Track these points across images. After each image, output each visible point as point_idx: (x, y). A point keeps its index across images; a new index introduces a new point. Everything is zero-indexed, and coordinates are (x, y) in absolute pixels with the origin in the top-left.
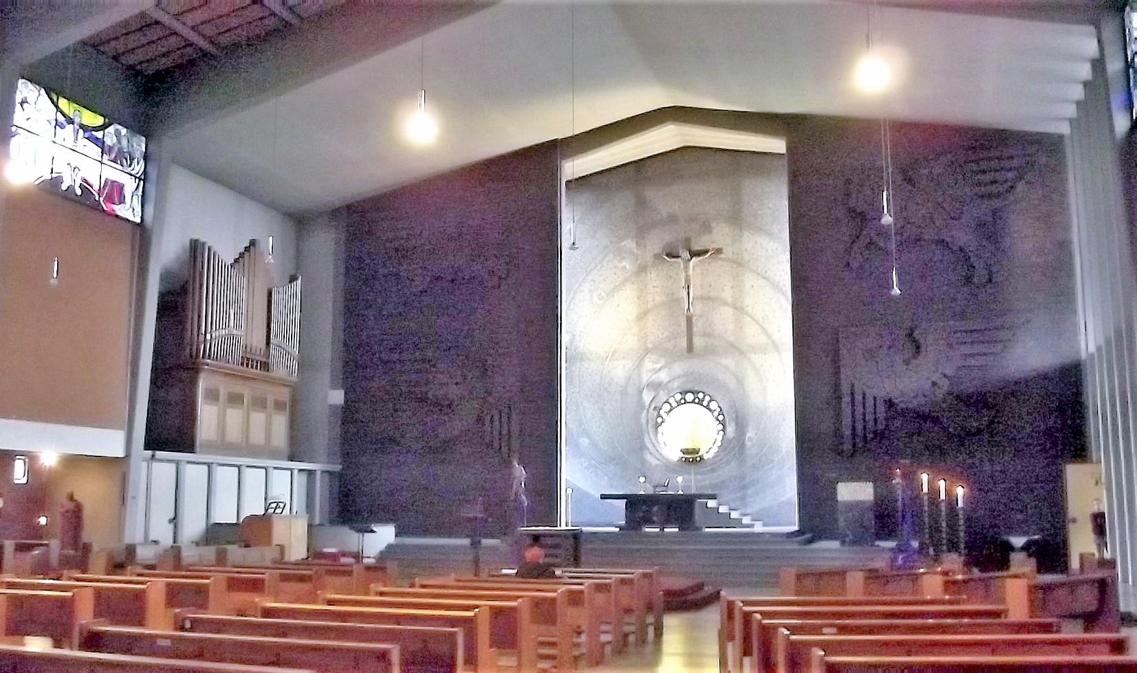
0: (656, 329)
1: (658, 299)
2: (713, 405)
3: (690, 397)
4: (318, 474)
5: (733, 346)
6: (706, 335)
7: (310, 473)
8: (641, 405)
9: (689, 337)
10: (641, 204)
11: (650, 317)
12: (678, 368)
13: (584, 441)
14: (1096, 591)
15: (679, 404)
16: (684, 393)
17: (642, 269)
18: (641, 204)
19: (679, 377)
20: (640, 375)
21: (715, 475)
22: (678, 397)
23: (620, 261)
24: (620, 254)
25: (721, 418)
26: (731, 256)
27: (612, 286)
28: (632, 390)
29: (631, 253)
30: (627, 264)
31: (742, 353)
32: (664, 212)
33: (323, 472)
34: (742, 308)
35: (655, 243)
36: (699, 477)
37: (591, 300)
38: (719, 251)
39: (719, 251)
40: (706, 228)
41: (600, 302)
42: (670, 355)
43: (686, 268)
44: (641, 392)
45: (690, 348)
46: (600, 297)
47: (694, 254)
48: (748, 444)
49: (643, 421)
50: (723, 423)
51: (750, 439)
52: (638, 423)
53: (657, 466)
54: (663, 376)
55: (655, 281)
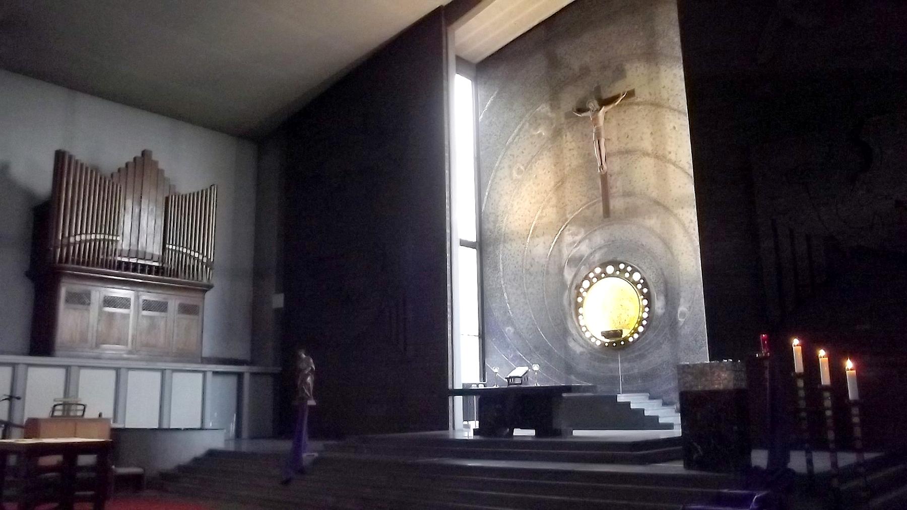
0: (577, 197)
2: (637, 277)
4: (247, 377)
5: (657, 203)
7: (240, 375)
11: (568, 185)
12: (599, 238)
15: (599, 278)
17: (557, 133)
18: (554, 63)
19: (600, 248)
20: (560, 251)
23: (536, 129)
24: (535, 121)
25: (645, 290)
26: (648, 97)
27: (529, 158)
28: (553, 270)
31: (667, 209)
32: (576, 65)
33: (253, 374)
34: (664, 157)
35: (568, 101)
37: (511, 175)
38: (631, 94)
39: (631, 94)
40: (620, 73)
41: (519, 177)
42: (585, 222)
44: (561, 270)
45: (607, 212)
46: (519, 172)
48: (681, 320)
49: (566, 303)
50: (648, 297)
51: (683, 314)
53: (582, 354)
54: (584, 249)
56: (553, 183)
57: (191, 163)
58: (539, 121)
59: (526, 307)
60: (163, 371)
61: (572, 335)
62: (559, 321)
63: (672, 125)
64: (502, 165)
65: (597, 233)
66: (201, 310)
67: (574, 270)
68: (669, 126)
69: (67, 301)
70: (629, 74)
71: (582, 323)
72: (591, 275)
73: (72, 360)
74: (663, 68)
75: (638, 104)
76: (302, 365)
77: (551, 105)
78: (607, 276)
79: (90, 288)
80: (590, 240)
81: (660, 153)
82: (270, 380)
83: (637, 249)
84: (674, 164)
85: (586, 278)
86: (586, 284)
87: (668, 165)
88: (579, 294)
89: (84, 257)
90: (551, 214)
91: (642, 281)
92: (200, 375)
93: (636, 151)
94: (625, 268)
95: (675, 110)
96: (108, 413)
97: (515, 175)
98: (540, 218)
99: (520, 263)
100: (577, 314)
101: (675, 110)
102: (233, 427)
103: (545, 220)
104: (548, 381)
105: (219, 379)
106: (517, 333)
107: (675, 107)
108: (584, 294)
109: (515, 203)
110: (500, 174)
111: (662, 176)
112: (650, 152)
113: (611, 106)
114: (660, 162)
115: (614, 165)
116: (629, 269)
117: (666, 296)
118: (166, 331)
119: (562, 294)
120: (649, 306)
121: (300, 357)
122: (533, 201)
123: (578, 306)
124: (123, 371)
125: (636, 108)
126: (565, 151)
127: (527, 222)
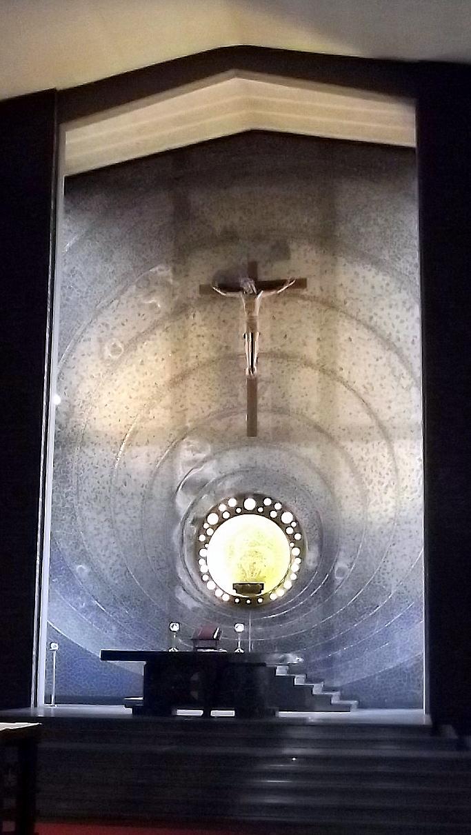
0: (201, 399)
2: (287, 518)
5: (319, 429)
11: (191, 382)
12: (232, 460)
15: (233, 513)
17: (180, 310)
18: (183, 213)
19: (233, 474)
20: (172, 470)
23: (150, 294)
24: (149, 286)
25: (298, 537)
26: (318, 293)
27: (133, 334)
28: (159, 492)
31: (331, 438)
32: (218, 225)
34: (333, 372)
35: (203, 269)
37: (101, 351)
38: (301, 283)
39: (301, 283)
40: (282, 251)
41: (115, 357)
42: (221, 441)
44: (172, 496)
45: (252, 429)
46: (115, 350)
48: (338, 578)
49: (175, 540)
50: (300, 545)
51: (342, 572)
53: (195, 610)
54: (209, 471)
56: (168, 376)
58: (154, 287)
59: (112, 540)
61: (182, 584)
62: (162, 564)
63: (347, 335)
64: (86, 336)
65: (230, 453)
67: (192, 498)
68: (343, 337)
70: (294, 255)
71: (203, 569)
72: (222, 508)
74: (342, 260)
75: (303, 298)
77: (174, 270)
78: (245, 512)
80: (219, 460)
81: (328, 366)
83: (286, 482)
84: (345, 384)
85: (215, 510)
86: (213, 519)
87: (338, 383)
88: (202, 531)
90: (161, 417)
91: (294, 524)
93: (295, 357)
94: (273, 505)
95: (352, 317)
97: (107, 353)
98: (143, 419)
99: (107, 477)
100: (197, 557)
101: (352, 317)
103: (152, 424)
104: (141, 642)
106: (96, 575)
107: (354, 314)
108: (210, 532)
109: (105, 394)
110: (82, 347)
111: (328, 399)
112: (314, 361)
113: (273, 293)
114: (328, 379)
115: (264, 370)
116: (278, 506)
117: (321, 548)
119: (172, 528)
120: (301, 556)
122: (134, 395)
123: (197, 547)
125: (300, 301)
126: (190, 336)
127: (123, 422)
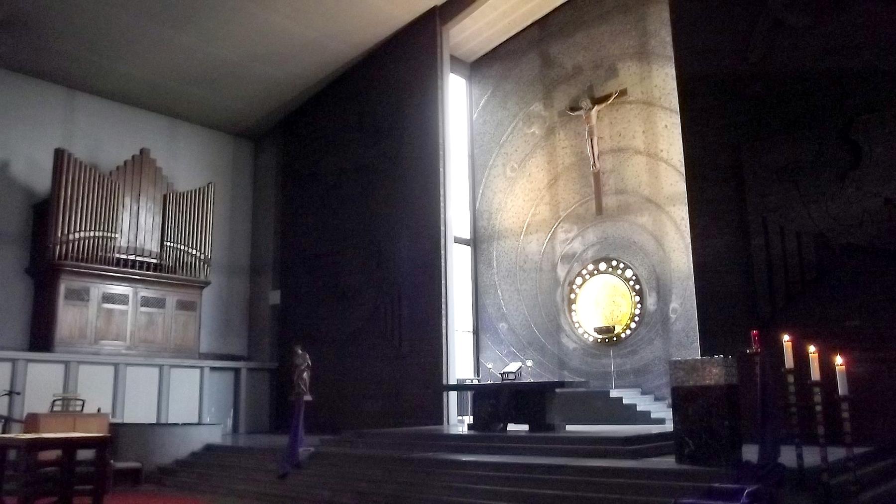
0: (570, 195)
1: (568, 161)
2: (629, 273)
3: (603, 266)
4: (244, 373)
5: (649, 201)
6: (620, 192)
7: (237, 371)
8: (556, 280)
9: (598, 198)
10: (547, 62)
11: (561, 183)
12: (591, 236)
13: (503, 326)
14: (604, 205)
15: (592, 274)
16: (596, 262)
17: (550, 132)
18: (547, 62)
19: (593, 245)
20: (553, 248)
21: (637, 357)
22: (591, 267)
23: (530, 127)
24: (529, 120)
25: (637, 287)
26: (640, 96)
27: (523, 156)
28: (546, 266)
29: (540, 116)
30: (536, 130)
31: (658, 206)
32: (569, 65)
33: (250, 370)
34: (656, 155)
35: (562, 100)
36: (618, 360)
37: (505, 173)
38: (623, 93)
39: (623, 93)
40: (613, 72)
41: (513, 175)
42: (578, 220)
43: (588, 118)
44: (554, 267)
45: (600, 210)
46: (513, 170)
47: (597, 101)
48: (673, 316)
49: (559, 299)
50: (640, 293)
51: (675, 311)
52: (555, 301)
53: (575, 349)
54: (577, 246)
55: (563, 140)
56: (546, 181)
57: (189, 161)
58: (533, 120)
59: (519, 303)
60: (161, 367)
61: (565, 331)
62: (552, 318)
63: (664, 124)
64: (496, 163)
65: (590, 230)
66: (198, 306)
67: (567, 267)
68: (661, 125)
69: (66, 297)
70: (622, 73)
71: (575, 320)
72: (584, 272)
73: (71, 356)
74: (655, 67)
75: (630, 103)
76: (299, 361)
77: (544, 104)
78: (600, 272)
79: (88, 285)
80: (583, 237)
81: (652, 151)
82: (267, 376)
83: (629, 246)
84: (666, 162)
85: (579, 274)
86: (579, 280)
87: (659, 163)
88: (572, 291)
89: (83, 254)
90: (544, 211)
91: (634, 278)
92: (198, 371)
93: (628, 149)
94: (618, 265)
95: (667, 109)
96: (107, 409)
97: (509, 173)
98: (534, 215)
99: (514, 260)
100: (570, 311)
101: (667, 109)
102: (230, 422)
103: (538, 218)
104: (541, 376)
105: (216, 375)
106: (511, 329)
107: (667, 105)
108: (577, 291)
109: (509, 201)
110: (494, 172)
111: (654, 174)
112: (642, 150)
113: (604, 105)
114: (652, 161)
115: (607, 164)
116: (622, 266)
117: (658, 293)
118: (164, 327)
119: (555, 291)
120: (641, 302)
121: (296, 353)
122: (527, 198)
123: (571, 302)
124: (121, 367)
125: (628, 106)
126: (558, 149)
127: (521, 219)
